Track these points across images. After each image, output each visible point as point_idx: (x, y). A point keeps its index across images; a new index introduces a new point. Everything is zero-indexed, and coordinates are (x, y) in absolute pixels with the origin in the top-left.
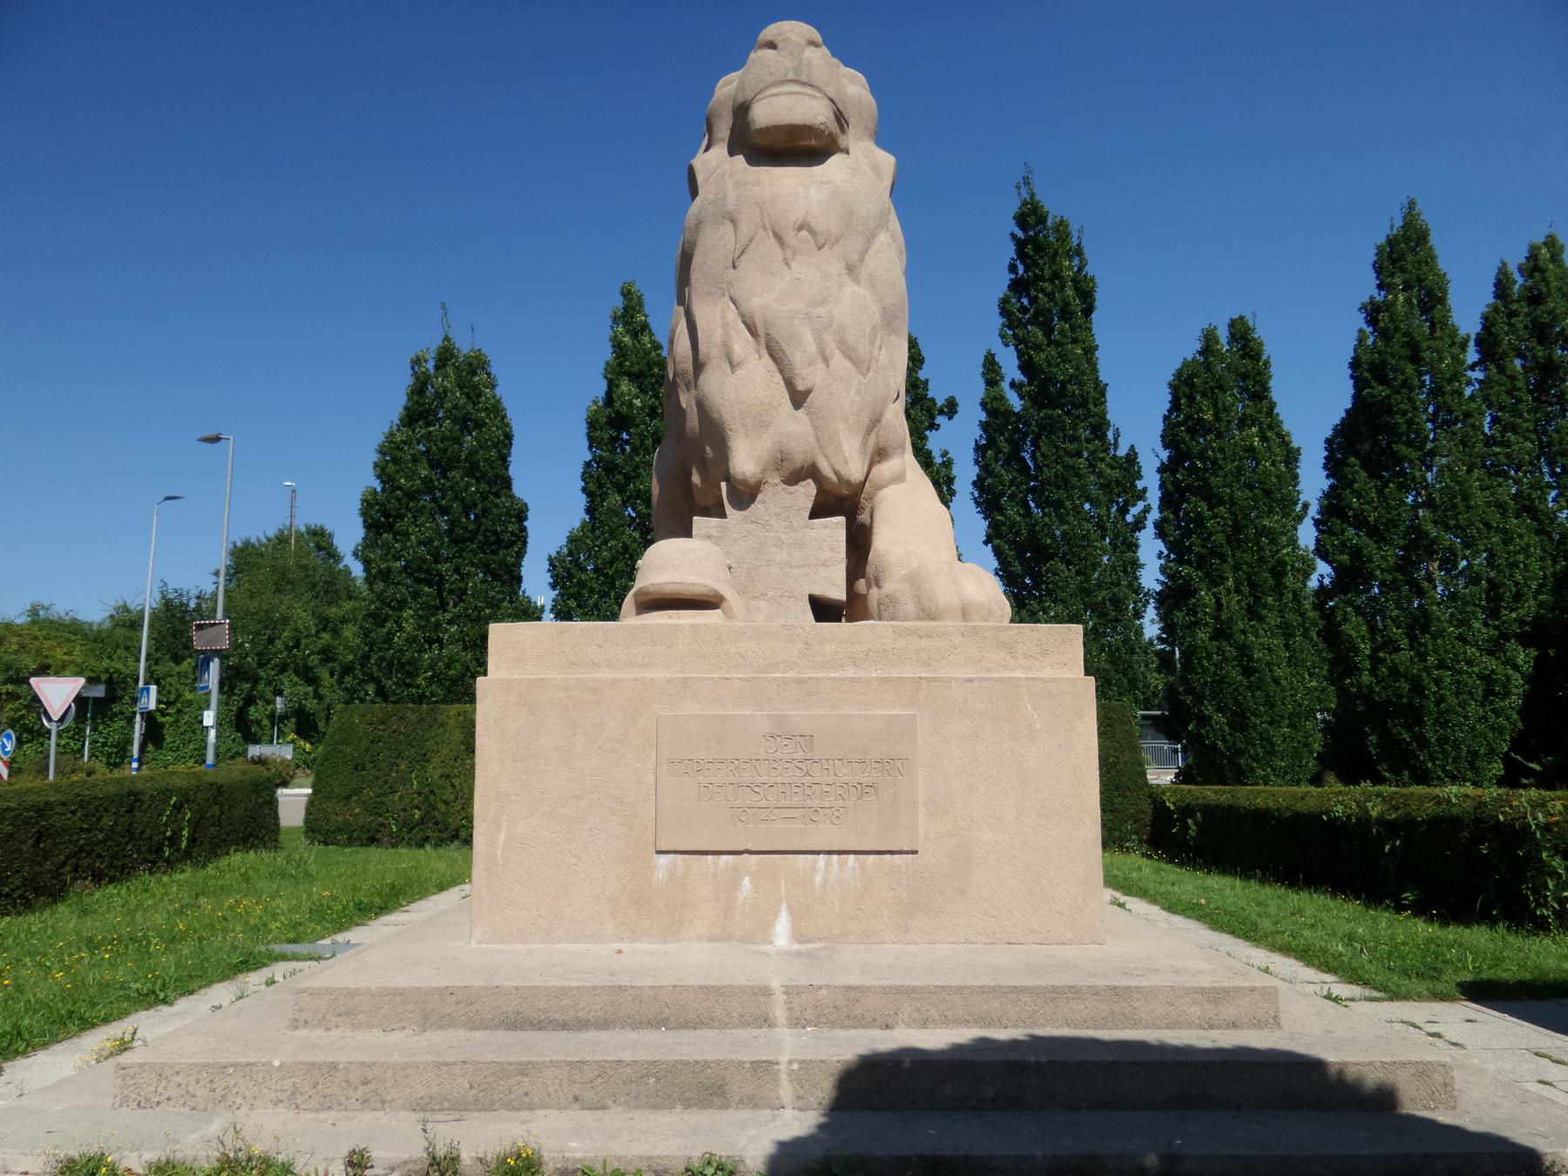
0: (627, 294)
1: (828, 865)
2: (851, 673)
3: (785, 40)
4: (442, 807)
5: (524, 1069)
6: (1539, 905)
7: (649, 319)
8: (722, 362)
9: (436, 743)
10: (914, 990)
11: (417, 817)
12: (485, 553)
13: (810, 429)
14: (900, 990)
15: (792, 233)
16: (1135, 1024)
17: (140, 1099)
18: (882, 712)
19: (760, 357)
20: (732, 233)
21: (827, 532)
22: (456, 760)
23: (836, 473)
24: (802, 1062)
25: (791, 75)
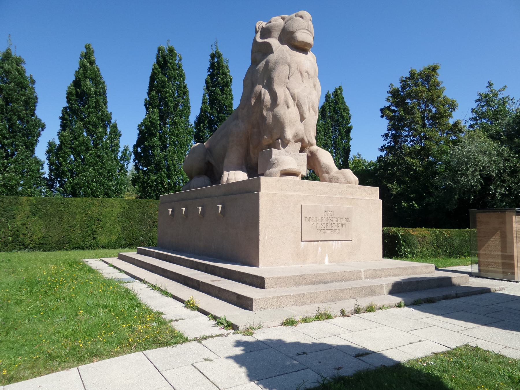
0: (88, 48)
1: (335, 244)
2: (338, 196)
3: (306, 17)
4: (22, 236)
5: (341, 291)
6: (400, 252)
7: (96, 60)
8: (284, 106)
9: (19, 211)
10: (385, 269)
11: (10, 240)
12: (25, 138)
13: (304, 129)
14: (382, 270)
15: (304, 73)
16: (416, 274)
17: (260, 308)
18: (345, 206)
19: (295, 106)
20: (288, 69)
21: (303, 157)
22: (27, 218)
23: (309, 141)
24: (387, 284)
25: (306, 28)
